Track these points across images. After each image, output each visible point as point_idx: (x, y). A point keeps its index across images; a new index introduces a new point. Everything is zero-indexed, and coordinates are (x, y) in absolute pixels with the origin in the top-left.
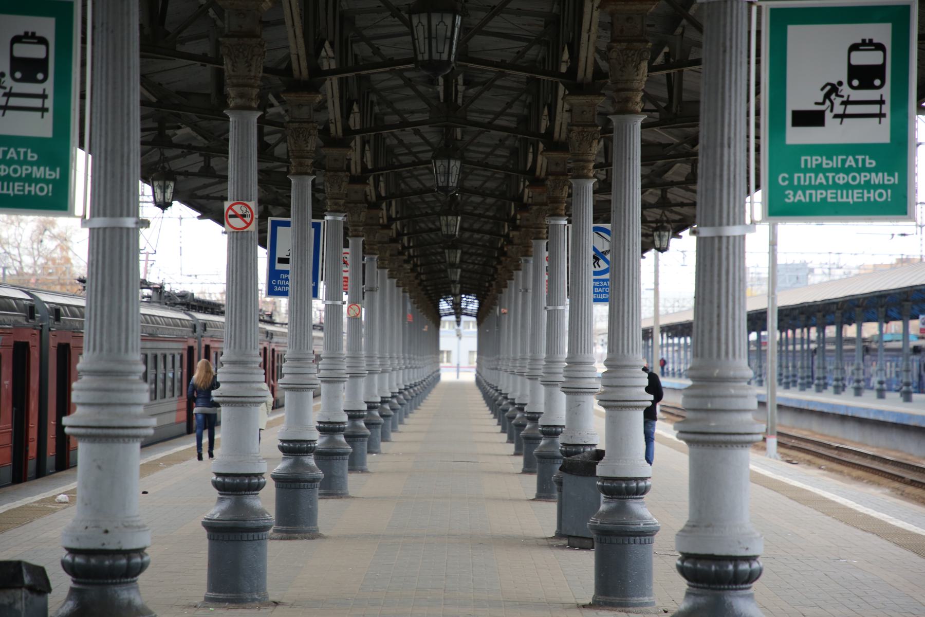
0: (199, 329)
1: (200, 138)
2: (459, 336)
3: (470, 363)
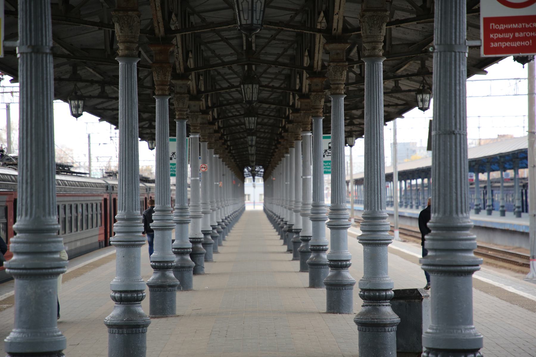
0: (148, 190)
1: (97, 75)
2: (254, 187)
3: (260, 200)
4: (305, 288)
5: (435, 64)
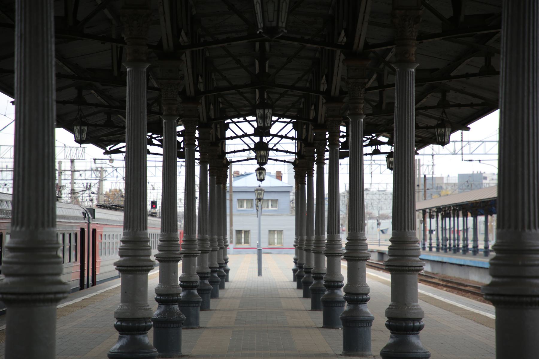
4: (318, 328)
5: (502, 64)
